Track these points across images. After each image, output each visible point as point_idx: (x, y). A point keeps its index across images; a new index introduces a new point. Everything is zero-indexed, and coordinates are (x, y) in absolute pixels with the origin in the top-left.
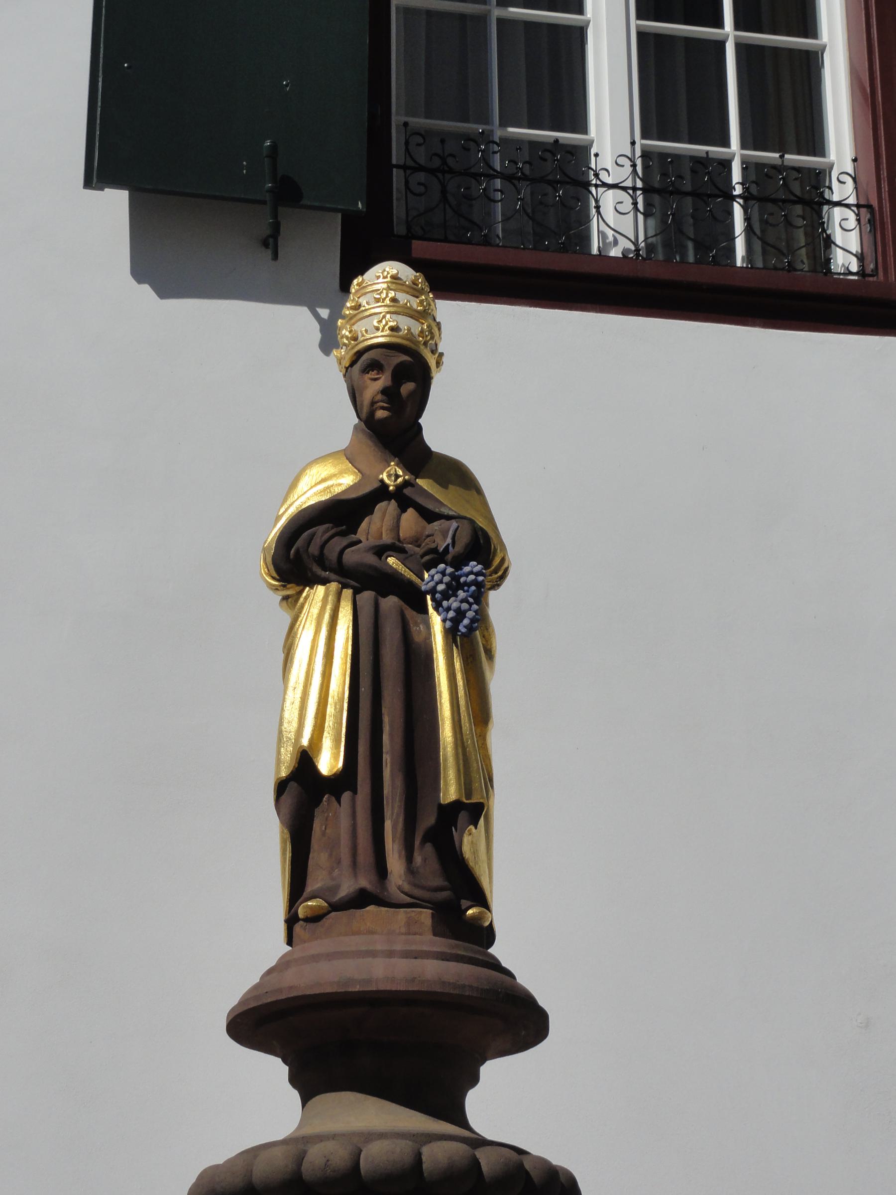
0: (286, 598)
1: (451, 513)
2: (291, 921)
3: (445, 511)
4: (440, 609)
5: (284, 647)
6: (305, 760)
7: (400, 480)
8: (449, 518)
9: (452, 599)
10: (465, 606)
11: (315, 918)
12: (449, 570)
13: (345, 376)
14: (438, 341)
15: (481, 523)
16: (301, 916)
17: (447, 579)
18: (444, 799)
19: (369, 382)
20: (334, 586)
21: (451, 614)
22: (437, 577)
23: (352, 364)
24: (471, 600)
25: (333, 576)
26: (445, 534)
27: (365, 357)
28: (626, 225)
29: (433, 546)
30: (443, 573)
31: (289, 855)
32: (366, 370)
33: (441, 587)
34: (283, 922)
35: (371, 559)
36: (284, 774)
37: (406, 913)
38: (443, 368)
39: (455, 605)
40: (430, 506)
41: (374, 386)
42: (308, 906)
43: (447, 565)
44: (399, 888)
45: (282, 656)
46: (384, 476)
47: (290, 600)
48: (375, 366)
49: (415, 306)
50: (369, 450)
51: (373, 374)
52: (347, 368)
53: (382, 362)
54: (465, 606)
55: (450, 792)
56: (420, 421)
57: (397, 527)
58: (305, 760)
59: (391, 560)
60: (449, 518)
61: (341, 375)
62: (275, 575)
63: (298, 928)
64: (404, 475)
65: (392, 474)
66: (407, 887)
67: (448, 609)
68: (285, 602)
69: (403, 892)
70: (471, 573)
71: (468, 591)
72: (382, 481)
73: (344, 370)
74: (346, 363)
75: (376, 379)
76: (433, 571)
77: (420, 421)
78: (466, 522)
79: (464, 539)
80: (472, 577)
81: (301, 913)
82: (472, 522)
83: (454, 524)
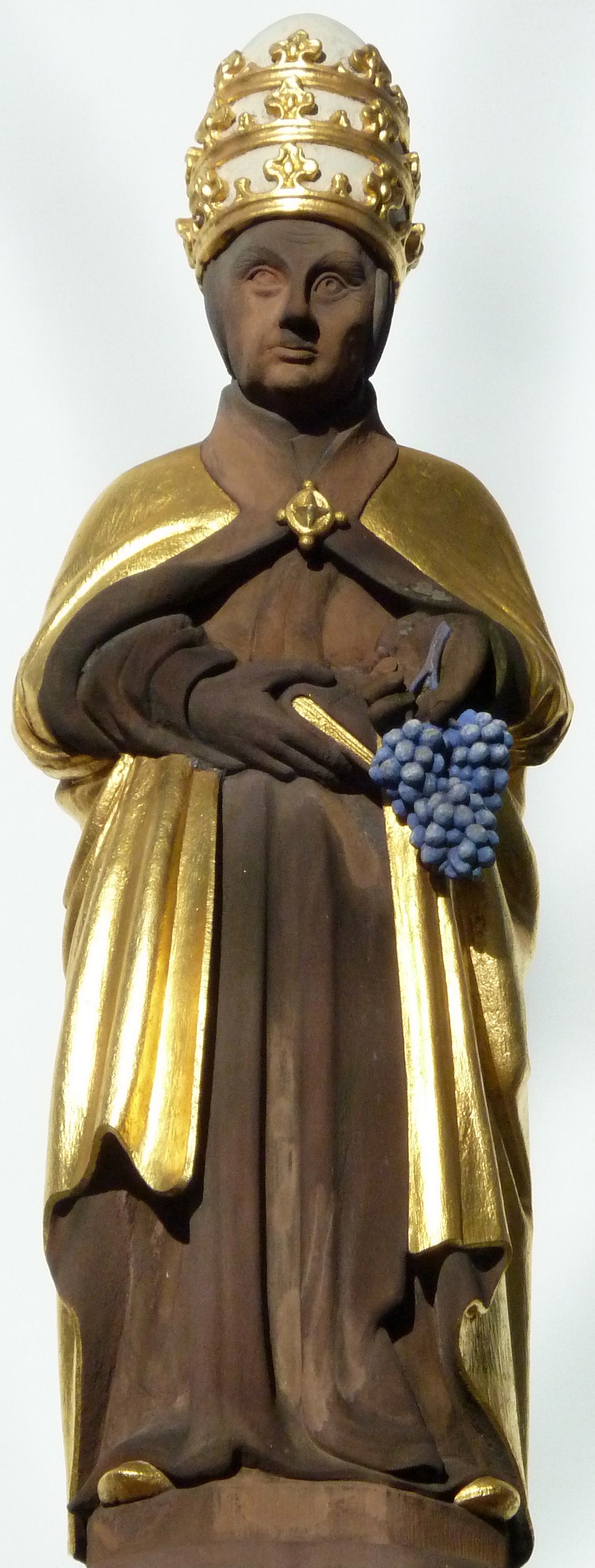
0: (68, 785)
1: (438, 597)
2: (83, 1509)
3: (421, 590)
4: (411, 817)
5: (68, 893)
6: (110, 1160)
7: (326, 519)
8: (436, 610)
9: (436, 797)
10: (463, 814)
11: (134, 1494)
12: (431, 732)
13: (201, 280)
14: (411, 200)
15: (506, 614)
16: (103, 1496)
17: (424, 754)
18: (416, 1245)
19: (253, 300)
20: (179, 761)
21: (433, 831)
22: (403, 749)
23: (216, 253)
24: (476, 799)
25: (171, 739)
26: (422, 649)
27: (244, 242)
28: (469, 733)
29: (393, 679)
30: (416, 740)
31: (76, 1363)
32: (249, 271)
33: (411, 771)
34: (66, 1512)
35: (258, 706)
36: (65, 1187)
37: (330, 1491)
38: (423, 259)
39: (443, 811)
40: (389, 580)
41: (266, 310)
42: (121, 1475)
43: (422, 720)
44: (317, 1438)
45: (61, 914)
46: (288, 514)
47: (79, 790)
48: (266, 262)
49: (358, 125)
50: (262, 441)
51: (264, 281)
52: (205, 265)
53: (284, 256)
54: (463, 814)
55: (430, 1224)
56: (371, 379)
57: (313, 630)
58: (110, 1160)
59: (307, 709)
60: (436, 610)
61: (192, 275)
62: (44, 734)
63: (96, 1526)
64: (333, 511)
65: (308, 510)
66: (332, 1437)
67: (426, 821)
68: (67, 797)
69: (323, 1447)
70: (480, 738)
71: (470, 779)
72: (284, 523)
73: (198, 268)
74: (202, 251)
75: (267, 295)
76: (393, 735)
77: (371, 379)
78: (467, 621)
79: (466, 666)
80: (480, 749)
81: (103, 1487)
82: (481, 619)
83: (443, 628)
